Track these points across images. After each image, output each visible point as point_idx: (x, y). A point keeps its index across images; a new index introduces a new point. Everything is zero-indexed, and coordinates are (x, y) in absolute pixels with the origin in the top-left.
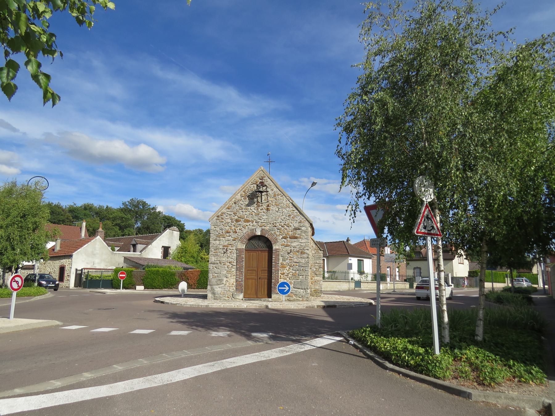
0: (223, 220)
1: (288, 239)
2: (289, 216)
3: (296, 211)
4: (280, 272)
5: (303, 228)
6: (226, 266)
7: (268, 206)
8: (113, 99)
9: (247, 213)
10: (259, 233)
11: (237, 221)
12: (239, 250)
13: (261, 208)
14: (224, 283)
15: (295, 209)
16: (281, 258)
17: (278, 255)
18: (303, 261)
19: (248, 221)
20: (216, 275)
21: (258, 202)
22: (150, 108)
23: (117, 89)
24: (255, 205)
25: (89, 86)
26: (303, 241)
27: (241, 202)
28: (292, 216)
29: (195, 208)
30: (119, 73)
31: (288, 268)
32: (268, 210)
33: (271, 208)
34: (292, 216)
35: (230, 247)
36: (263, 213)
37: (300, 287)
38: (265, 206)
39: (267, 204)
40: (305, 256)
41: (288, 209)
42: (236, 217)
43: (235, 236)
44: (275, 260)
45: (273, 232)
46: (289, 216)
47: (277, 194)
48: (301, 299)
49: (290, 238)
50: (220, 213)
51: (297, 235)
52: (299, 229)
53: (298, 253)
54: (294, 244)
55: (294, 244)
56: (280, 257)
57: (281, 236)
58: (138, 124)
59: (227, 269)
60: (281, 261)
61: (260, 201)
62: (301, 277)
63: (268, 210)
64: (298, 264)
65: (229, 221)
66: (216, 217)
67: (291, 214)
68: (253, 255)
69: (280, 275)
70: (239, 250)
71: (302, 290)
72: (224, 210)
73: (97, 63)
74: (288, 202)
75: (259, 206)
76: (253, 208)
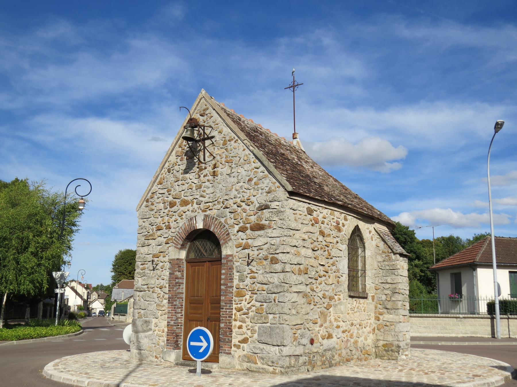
0: (153, 207)
1: (249, 232)
2: (250, 180)
3: (262, 168)
4: (234, 306)
5: (273, 205)
6: (155, 295)
7: (215, 166)
8: (351, 81)
9: (184, 187)
10: (200, 226)
11: (172, 205)
12: (175, 264)
13: (205, 172)
14: (153, 328)
15: (259, 164)
16: (236, 276)
17: (231, 268)
18: (275, 279)
19: (185, 203)
20: (142, 312)
21: (200, 162)
22: (399, 81)
23: (354, 67)
24: (195, 169)
25: (322, 72)
26: (275, 233)
27: (176, 168)
28: (255, 180)
29: (455, 210)
30: (355, 46)
31: (247, 297)
32: (214, 174)
33: (219, 170)
34: (255, 180)
35: (161, 258)
36: (207, 184)
37: (269, 340)
38: (210, 169)
39: (213, 162)
40: (278, 267)
41: (246, 167)
42: (170, 198)
43: (169, 234)
44: (226, 279)
45: (223, 220)
46: (250, 180)
47: (228, 138)
48: (271, 369)
49: (252, 229)
50: (150, 194)
51: (263, 222)
52: (267, 207)
53: (265, 262)
54: (259, 242)
55: (259, 242)
56: (235, 271)
57: (237, 228)
58: (381, 105)
59: (157, 300)
60: (236, 282)
61: (202, 159)
62: (271, 316)
63: (214, 174)
64: (265, 287)
65: (161, 206)
66: (145, 203)
67: (252, 176)
68: (199, 269)
69: (234, 311)
70: (175, 264)
71: (273, 349)
72: (155, 188)
73: (327, 41)
74: (247, 152)
75: (201, 170)
76: (192, 176)
